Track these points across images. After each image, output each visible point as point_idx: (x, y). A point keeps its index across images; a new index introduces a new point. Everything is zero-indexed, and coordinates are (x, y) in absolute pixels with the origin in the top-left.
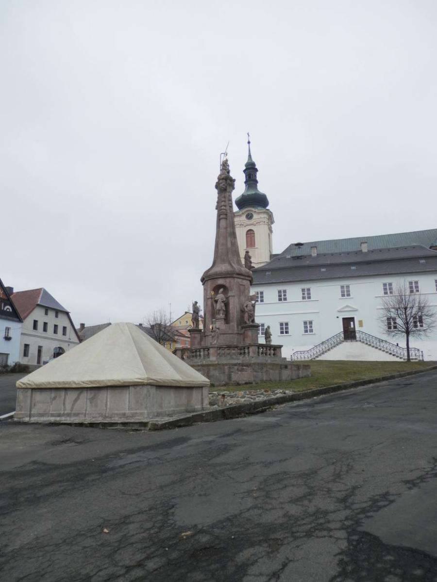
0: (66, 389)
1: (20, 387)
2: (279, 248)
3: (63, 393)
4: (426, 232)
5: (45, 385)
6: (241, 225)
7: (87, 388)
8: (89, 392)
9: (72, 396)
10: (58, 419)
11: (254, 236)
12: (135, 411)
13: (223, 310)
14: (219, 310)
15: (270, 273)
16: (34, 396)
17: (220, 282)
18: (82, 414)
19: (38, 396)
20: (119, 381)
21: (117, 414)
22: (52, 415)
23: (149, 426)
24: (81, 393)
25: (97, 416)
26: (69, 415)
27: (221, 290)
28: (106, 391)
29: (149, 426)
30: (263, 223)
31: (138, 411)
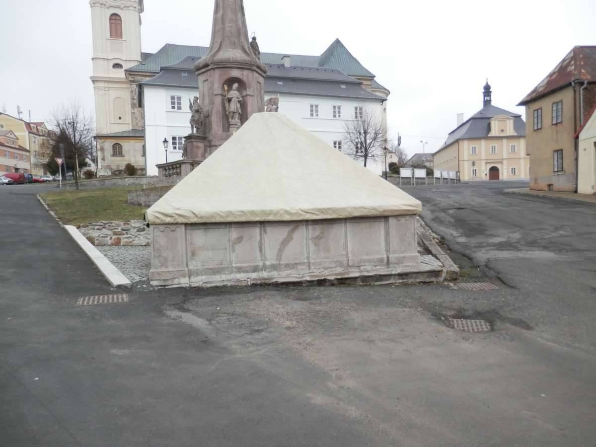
0: (263, 223)
1: (158, 221)
2: (152, 47)
3: (257, 231)
4: (587, 51)
5: (221, 216)
6: (101, 4)
7: (307, 222)
8: (310, 227)
9: (275, 236)
10: (265, 274)
11: (121, 24)
12: (402, 255)
13: (239, 113)
14: (234, 113)
15: (186, 75)
16: (189, 237)
17: (235, 73)
18: (304, 264)
19: (199, 237)
20: (374, 209)
21: (369, 261)
22: (240, 270)
23: (444, 275)
24: (293, 230)
25: (333, 265)
26: (274, 267)
27: (236, 85)
28: (343, 224)
29: (444, 275)
30: (134, 9)
31: (407, 255)
